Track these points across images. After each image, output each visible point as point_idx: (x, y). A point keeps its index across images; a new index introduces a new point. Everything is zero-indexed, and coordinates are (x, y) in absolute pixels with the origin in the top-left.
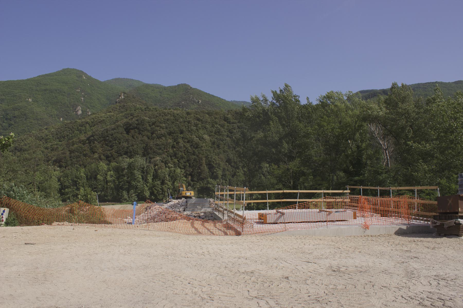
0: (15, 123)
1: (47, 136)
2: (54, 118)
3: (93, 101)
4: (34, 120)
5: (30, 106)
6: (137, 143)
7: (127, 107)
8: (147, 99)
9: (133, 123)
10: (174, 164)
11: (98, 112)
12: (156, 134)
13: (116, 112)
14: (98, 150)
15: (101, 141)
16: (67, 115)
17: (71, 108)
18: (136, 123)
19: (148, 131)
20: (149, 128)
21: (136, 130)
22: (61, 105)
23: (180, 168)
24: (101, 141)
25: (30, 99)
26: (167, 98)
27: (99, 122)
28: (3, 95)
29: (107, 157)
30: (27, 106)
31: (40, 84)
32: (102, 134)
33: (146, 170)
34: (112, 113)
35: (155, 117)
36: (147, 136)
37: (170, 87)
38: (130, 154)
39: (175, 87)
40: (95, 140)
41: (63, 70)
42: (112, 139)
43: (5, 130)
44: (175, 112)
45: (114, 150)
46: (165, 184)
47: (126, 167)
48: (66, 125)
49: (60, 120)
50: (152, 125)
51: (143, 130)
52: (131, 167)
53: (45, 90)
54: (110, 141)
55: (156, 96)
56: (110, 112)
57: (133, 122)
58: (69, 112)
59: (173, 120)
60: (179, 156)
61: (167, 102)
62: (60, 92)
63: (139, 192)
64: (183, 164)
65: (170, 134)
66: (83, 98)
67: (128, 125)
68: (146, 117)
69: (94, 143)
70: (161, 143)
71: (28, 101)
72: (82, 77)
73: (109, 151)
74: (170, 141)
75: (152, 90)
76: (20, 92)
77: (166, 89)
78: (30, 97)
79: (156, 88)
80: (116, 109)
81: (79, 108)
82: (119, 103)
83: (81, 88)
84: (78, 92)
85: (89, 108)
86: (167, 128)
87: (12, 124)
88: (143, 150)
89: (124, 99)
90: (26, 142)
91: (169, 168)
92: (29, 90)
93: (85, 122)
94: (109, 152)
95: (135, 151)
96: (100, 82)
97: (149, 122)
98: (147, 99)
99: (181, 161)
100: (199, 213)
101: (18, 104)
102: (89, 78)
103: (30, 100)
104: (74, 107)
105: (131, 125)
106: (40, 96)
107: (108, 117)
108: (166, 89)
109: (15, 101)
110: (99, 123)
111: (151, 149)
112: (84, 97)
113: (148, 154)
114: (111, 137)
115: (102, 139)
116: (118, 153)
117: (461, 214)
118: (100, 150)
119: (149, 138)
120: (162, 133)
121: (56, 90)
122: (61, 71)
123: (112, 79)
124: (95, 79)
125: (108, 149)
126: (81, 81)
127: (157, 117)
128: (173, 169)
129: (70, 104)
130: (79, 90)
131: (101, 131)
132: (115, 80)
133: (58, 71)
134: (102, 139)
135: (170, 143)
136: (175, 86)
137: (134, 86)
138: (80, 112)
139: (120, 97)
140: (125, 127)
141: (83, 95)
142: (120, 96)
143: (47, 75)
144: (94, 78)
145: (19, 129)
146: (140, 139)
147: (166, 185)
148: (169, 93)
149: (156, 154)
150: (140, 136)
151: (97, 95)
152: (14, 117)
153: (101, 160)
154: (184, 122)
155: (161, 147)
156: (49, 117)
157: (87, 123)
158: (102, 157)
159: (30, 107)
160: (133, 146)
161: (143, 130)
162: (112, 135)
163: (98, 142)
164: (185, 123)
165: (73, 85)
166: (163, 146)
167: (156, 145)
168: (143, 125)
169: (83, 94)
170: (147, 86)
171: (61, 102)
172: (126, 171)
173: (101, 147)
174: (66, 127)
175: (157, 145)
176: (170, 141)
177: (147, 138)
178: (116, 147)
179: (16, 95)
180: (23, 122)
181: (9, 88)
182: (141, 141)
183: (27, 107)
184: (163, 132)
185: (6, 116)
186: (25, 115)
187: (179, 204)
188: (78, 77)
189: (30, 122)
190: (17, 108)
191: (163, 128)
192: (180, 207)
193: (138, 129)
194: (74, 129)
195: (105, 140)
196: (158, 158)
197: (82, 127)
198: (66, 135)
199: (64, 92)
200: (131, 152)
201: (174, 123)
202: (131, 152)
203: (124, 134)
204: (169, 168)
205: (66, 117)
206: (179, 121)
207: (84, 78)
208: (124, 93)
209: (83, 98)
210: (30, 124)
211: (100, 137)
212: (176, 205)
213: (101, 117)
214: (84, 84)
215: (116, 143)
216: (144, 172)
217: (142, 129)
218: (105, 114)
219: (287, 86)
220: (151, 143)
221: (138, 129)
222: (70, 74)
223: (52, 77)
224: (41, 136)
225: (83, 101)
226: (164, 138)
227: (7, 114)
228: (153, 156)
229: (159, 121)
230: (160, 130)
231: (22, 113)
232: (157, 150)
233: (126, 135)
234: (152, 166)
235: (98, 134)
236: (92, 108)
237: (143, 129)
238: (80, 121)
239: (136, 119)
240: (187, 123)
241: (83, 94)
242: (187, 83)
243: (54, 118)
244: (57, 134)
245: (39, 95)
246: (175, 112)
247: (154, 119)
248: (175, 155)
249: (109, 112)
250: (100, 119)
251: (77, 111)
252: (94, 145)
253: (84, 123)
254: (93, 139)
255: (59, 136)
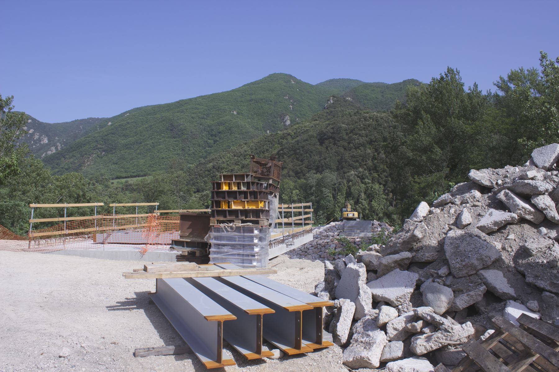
0: (220, 139)
1: (246, 151)
2: (260, 132)
3: (304, 109)
4: (239, 134)
5: (235, 119)
6: (331, 155)
7: (335, 113)
8: (366, 102)
9: (327, 132)
10: (373, 180)
11: (302, 121)
12: (353, 144)
13: (322, 120)
14: (288, 165)
15: (291, 155)
16: (274, 127)
17: (279, 119)
18: (331, 131)
19: (343, 139)
20: (346, 137)
21: (330, 139)
22: (267, 116)
23: (380, 184)
24: (291, 155)
25: (234, 112)
26: (390, 98)
27: (302, 133)
28: (209, 110)
29: (297, 173)
30: (232, 119)
31: (245, 94)
32: (292, 147)
33: (338, 187)
34: (317, 122)
35: (354, 123)
36: (343, 147)
37: (394, 84)
38: (319, 169)
39: (400, 84)
40: (285, 154)
41: (270, 76)
42: (303, 152)
43: (211, 147)
44: (379, 115)
45: (304, 165)
46: (359, 204)
47: (315, 184)
48: (266, 139)
49: (267, 133)
50: (350, 133)
51: (339, 139)
52: (320, 184)
53: (251, 100)
54: (301, 155)
55: (376, 98)
56: (316, 120)
57: (327, 130)
58: (277, 123)
59: (375, 125)
60: (380, 169)
61: (390, 103)
62: (267, 101)
63: (329, 213)
64: (384, 178)
65: (371, 142)
66: (291, 106)
67: (322, 135)
68: (343, 123)
69: (283, 158)
70: (358, 154)
71: (233, 114)
72: (290, 81)
73: (299, 166)
74: (369, 151)
75: (372, 91)
76: (225, 105)
77: (388, 88)
78: (235, 110)
79: (377, 88)
80: (323, 116)
81: (287, 117)
82: (327, 109)
83: (289, 94)
84: (286, 100)
85: (298, 117)
86: (367, 136)
87: (217, 141)
88: (338, 163)
89: (333, 103)
90: (224, 160)
91: (365, 184)
92: (234, 102)
93: (286, 134)
94: (299, 167)
95: (328, 165)
96: (311, 86)
97: (346, 130)
98: (366, 102)
99: (382, 176)
100: (354, 239)
101: (223, 118)
102: (299, 82)
103: (235, 113)
104: (282, 117)
105: (325, 134)
106: (246, 107)
107: (312, 127)
108: (388, 88)
109: (220, 115)
110: (302, 134)
111: (346, 162)
112: (293, 104)
113: (342, 168)
114: (301, 149)
115: (292, 152)
116: (308, 168)
117: (183, 239)
118: (290, 165)
119: (345, 149)
120: (361, 142)
121: (262, 100)
122: (268, 77)
123: (326, 81)
124: (306, 83)
125: (298, 164)
126: (290, 86)
127: (356, 122)
128: (370, 185)
129: (277, 114)
130: (287, 98)
131: (291, 143)
132: (329, 82)
133: (264, 78)
134: (292, 152)
135: (369, 154)
136: (400, 83)
137: (351, 87)
138: (288, 123)
139: (329, 102)
140: (318, 137)
141: (291, 102)
142: (328, 101)
143: (252, 83)
144: (304, 81)
145: (224, 145)
146: (334, 150)
147: (360, 205)
148: (393, 92)
149: (351, 168)
150: (335, 147)
151: (307, 101)
152: (219, 133)
153: (289, 176)
154: (390, 127)
155: (358, 159)
156: (255, 130)
157: (289, 134)
158: (291, 173)
159: (235, 120)
160: (325, 159)
161: (339, 139)
162: (303, 147)
163: (288, 157)
164: (390, 129)
165: (279, 92)
166: (360, 158)
167: (352, 157)
168: (339, 134)
169: (291, 101)
170: (366, 86)
171: (267, 113)
172: (314, 188)
173: (291, 162)
174: (266, 141)
175: (353, 157)
176: (369, 151)
177: (343, 149)
178: (307, 160)
179: (221, 109)
180: (228, 137)
181: (214, 102)
182: (335, 153)
183: (232, 121)
184: (362, 140)
185: (212, 132)
186: (230, 130)
187: (336, 228)
188: (285, 82)
189: (235, 137)
190: (222, 123)
191: (362, 136)
192: (336, 231)
193: (334, 138)
194: (274, 142)
195: (296, 154)
196: (352, 172)
197: (283, 139)
198: (265, 150)
199: (271, 101)
200: (322, 166)
201: (376, 129)
202: (322, 166)
203: (317, 145)
204: (365, 184)
205: (273, 129)
206: (382, 126)
207: (293, 82)
208: (334, 97)
209: (291, 106)
210: (234, 139)
211: (290, 151)
212: (332, 228)
213: (305, 127)
214: (293, 90)
215: (307, 156)
216: (336, 190)
217: (337, 139)
218: (310, 123)
219: (450, 71)
220: (347, 155)
221: (334, 138)
222: (277, 79)
223: (257, 85)
224: (240, 152)
225: (292, 109)
226: (362, 148)
227: (212, 130)
228: (348, 170)
229: (357, 128)
230: (358, 139)
231: (227, 128)
232: (353, 163)
233: (319, 147)
234: (345, 182)
235: (288, 147)
236: (302, 117)
237: (339, 138)
238: (281, 132)
239: (332, 126)
240: (392, 128)
241: (291, 101)
242: (415, 78)
243: (260, 131)
244: (256, 149)
245: (244, 106)
246: (379, 115)
247: (352, 126)
248: (375, 169)
249: (315, 121)
250: (303, 129)
251: (285, 121)
252: (284, 159)
253: (285, 135)
254: (282, 153)
255: (258, 151)
